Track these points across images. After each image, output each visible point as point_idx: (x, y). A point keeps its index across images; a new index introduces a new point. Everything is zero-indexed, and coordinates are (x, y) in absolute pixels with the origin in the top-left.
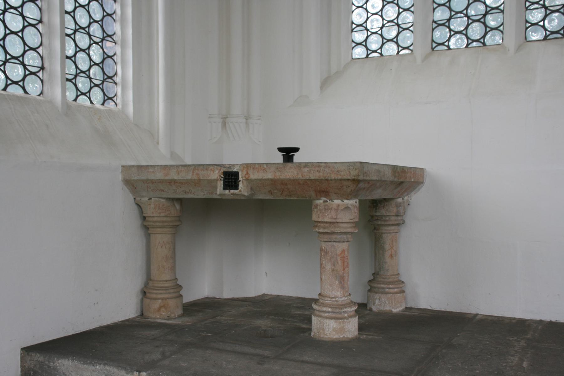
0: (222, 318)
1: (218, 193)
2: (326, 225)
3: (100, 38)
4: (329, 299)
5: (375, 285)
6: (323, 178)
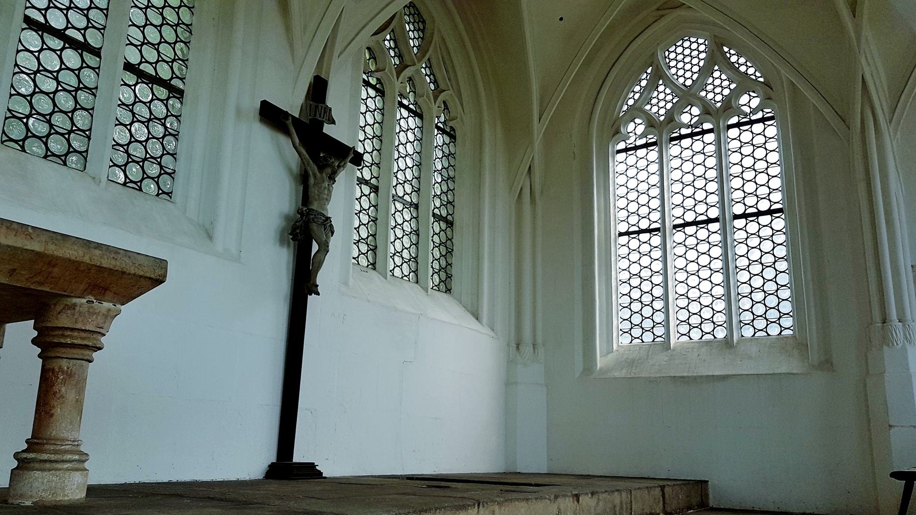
3: (171, 59)
6: (120, 270)
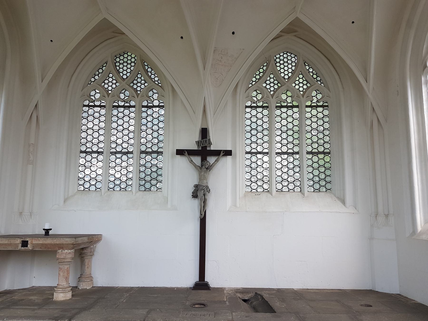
0: (15, 297)
1: (19, 249)
2: (62, 259)
4: (61, 286)
5: (81, 279)
